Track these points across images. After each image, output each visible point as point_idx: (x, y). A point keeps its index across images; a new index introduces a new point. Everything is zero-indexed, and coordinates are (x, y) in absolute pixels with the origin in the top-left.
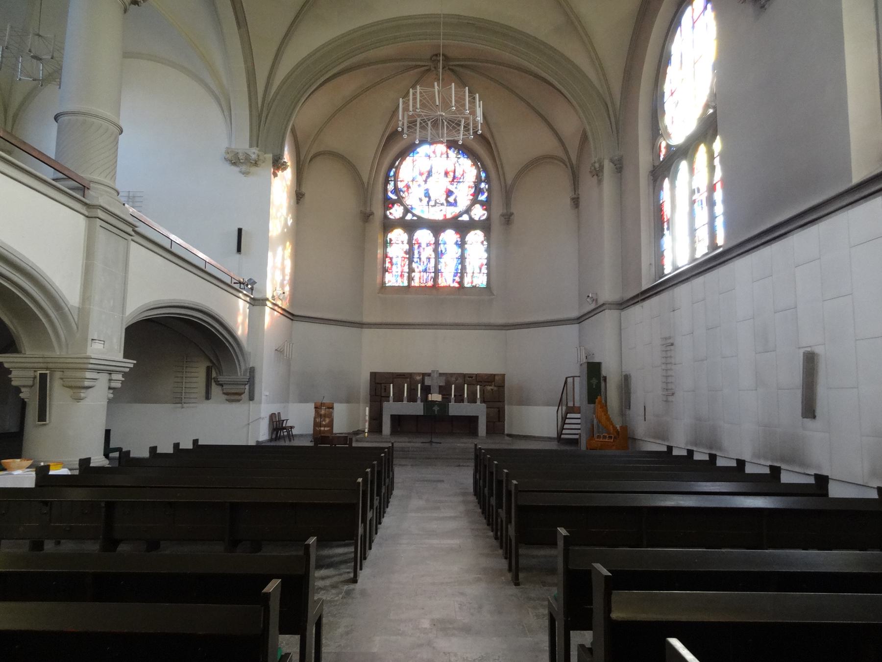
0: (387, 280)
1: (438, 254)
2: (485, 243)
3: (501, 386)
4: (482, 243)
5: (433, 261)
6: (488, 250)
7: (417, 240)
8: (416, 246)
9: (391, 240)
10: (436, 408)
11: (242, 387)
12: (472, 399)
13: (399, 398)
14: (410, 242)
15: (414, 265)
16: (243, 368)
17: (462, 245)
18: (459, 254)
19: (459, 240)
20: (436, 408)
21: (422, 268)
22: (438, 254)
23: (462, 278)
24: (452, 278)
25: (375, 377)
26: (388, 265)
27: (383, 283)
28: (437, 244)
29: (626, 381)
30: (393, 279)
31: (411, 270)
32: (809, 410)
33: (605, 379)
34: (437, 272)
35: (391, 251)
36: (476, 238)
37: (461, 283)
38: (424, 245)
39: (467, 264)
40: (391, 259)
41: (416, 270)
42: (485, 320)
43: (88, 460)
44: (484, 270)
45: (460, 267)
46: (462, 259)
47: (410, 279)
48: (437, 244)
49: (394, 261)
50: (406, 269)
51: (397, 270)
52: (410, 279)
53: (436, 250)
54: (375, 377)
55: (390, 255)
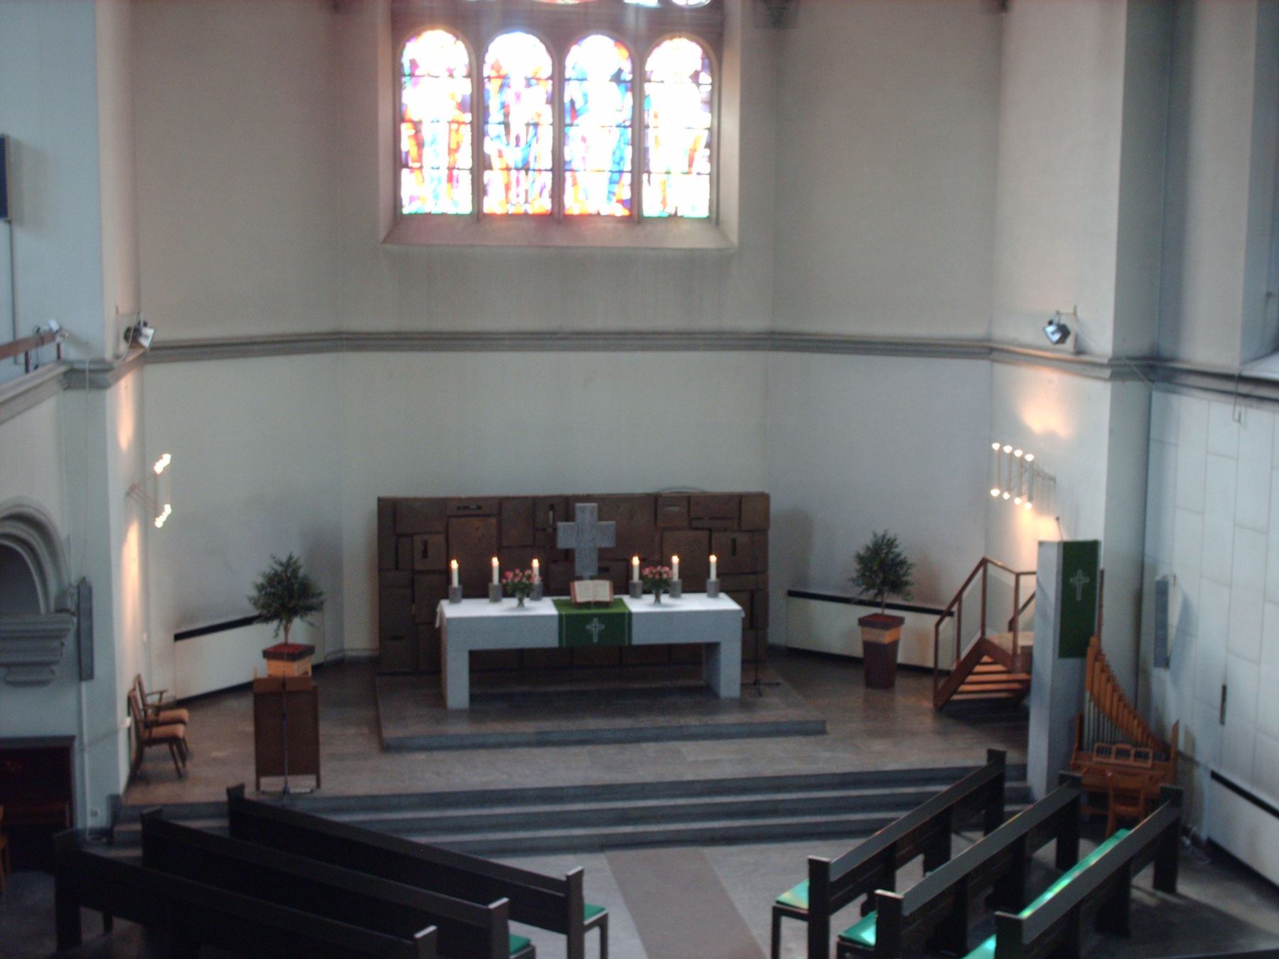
0: (405, 193)
1: (563, 112)
2: (705, 78)
3: (760, 531)
4: (695, 77)
5: (547, 133)
6: (714, 103)
7: (497, 67)
8: (492, 87)
9: (414, 64)
10: (595, 627)
11: (56, 644)
12: (694, 582)
13: (476, 587)
14: (476, 75)
15: (490, 147)
16: (53, 589)
17: (636, 84)
18: (627, 114)
19: (627, 66)
20: (595, 627)
21: (514, 156)
22: (563, 112)
23: (636, 187)
24: (604, 186)
25: (395, 519)
26: (407, 145)
27: (397, 202)
28: (559, 78)
29: (1151, 596)
30: (430, 191)
31: (481, 163)
32: (1222, 722)
33: (1102, 572)
34: (559, 168)
35: (413, 99)
36: (678, 58)
37: (634, 202)
38: (517, 83)
39: (650, 143)
40: (417, 125)
41: (496, 162)
42: (706, 322)
43: (241, 788)
44: (703, 164)
45: (628, 152)
46: (638, 126)
47: (479, 190)
48: (559, 78)
49: (426, 133)
50: (465, 159)
51: (435, 156)
52: (479, 190)
53: (556, 99)
54: (395, 519)
55: (412, 112)
